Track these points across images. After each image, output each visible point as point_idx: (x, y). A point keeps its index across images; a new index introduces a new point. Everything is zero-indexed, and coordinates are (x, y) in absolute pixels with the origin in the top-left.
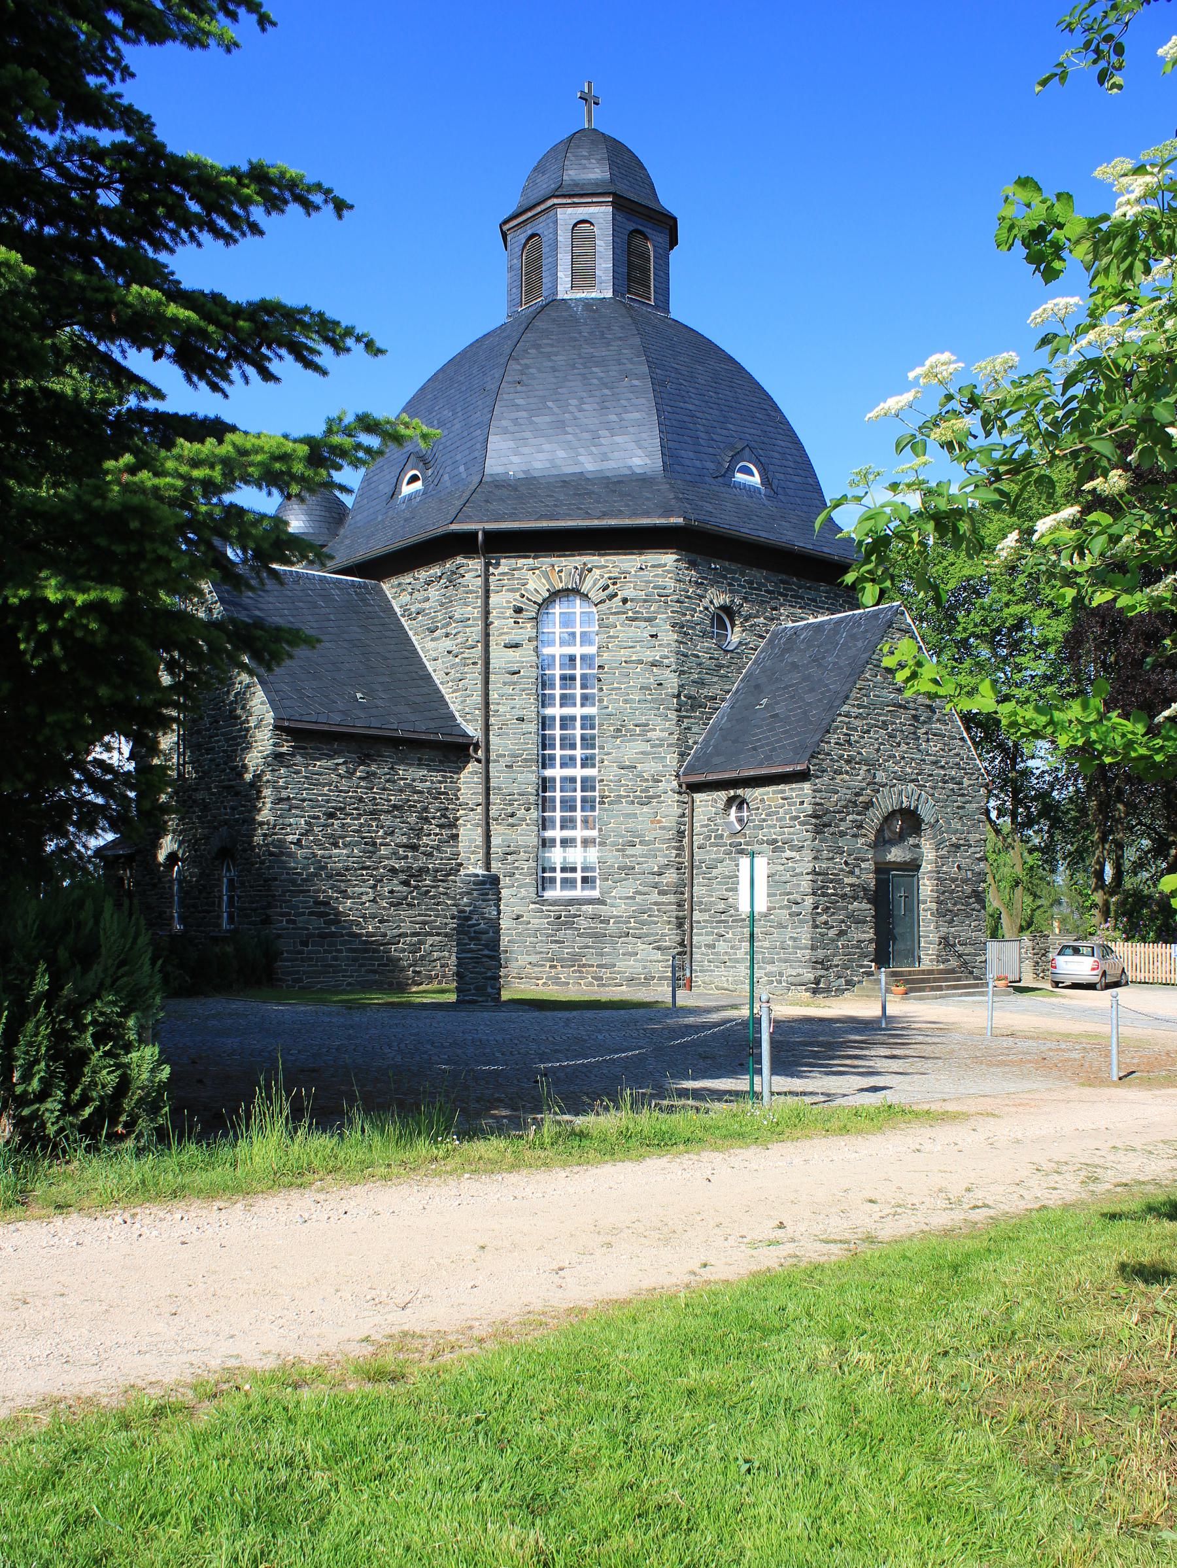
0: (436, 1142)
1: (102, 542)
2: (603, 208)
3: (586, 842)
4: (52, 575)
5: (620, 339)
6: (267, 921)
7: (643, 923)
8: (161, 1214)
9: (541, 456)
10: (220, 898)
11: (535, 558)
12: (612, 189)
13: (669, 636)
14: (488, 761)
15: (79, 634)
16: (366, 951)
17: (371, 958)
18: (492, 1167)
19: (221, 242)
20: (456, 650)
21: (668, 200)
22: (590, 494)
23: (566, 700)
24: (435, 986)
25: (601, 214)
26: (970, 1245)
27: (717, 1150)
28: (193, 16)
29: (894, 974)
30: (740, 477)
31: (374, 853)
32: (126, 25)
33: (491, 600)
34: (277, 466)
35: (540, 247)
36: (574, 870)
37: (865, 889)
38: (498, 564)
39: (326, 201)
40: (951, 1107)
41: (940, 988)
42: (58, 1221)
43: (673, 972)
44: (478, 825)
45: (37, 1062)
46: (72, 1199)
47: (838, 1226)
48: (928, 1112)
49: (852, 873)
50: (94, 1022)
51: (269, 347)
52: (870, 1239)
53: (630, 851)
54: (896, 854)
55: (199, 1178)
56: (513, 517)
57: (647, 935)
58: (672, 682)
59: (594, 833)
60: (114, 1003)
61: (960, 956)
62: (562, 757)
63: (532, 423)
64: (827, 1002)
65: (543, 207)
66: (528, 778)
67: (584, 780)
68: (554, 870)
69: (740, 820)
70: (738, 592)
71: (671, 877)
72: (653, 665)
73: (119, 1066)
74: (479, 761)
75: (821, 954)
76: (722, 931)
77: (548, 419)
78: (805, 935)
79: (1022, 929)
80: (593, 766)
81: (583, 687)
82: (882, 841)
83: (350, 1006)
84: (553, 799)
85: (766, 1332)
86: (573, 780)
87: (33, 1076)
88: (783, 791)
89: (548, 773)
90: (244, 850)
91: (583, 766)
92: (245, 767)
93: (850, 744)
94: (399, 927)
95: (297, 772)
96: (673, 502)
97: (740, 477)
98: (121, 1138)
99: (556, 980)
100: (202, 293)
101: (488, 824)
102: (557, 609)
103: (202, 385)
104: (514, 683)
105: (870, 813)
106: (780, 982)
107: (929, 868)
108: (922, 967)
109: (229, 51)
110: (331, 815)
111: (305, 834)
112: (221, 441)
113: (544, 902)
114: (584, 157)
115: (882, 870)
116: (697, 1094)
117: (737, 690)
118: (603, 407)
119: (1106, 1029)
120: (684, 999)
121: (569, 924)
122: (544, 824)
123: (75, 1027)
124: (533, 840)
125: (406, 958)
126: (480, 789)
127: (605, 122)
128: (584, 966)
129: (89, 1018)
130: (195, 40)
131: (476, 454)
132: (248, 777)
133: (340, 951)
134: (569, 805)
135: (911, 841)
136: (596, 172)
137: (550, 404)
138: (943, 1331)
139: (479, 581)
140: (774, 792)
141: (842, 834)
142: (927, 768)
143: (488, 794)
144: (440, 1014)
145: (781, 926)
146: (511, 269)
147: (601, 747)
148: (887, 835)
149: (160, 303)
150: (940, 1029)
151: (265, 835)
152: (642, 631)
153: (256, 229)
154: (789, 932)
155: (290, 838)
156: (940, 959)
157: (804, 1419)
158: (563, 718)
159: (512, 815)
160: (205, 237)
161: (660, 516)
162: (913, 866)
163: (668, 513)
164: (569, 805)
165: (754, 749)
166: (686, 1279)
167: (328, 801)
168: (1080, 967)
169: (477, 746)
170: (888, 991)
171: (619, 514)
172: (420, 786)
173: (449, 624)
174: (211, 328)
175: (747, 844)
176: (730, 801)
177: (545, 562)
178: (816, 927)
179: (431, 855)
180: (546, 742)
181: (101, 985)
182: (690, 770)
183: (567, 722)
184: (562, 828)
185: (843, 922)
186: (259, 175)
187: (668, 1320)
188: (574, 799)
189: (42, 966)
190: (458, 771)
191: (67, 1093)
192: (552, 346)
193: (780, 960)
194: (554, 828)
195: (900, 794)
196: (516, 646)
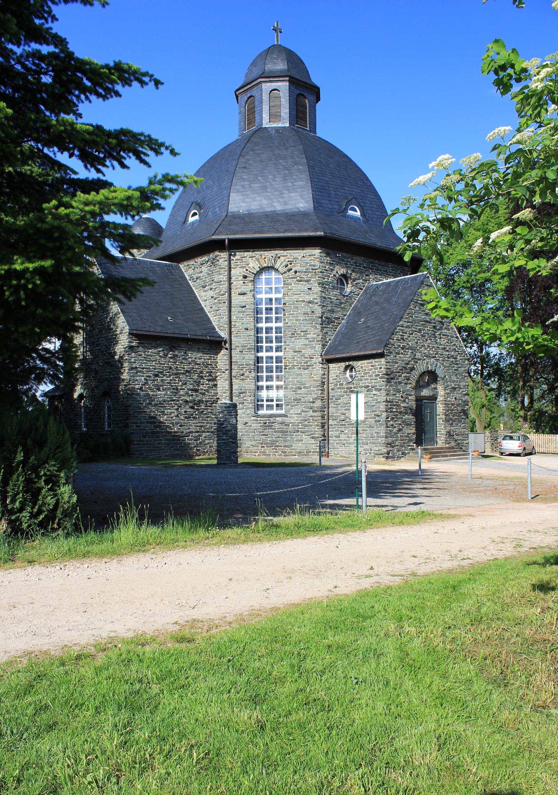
0: (208, 530)
1: (43, 241)
2: (284, 83)
3: (278, 387)
5: (293, 146)
6: (126, 426)
7: (305, 426)
8: (78, 565)
9: (255, 203)
10: (104, 415)
13: (317, 289)
14: (231, 349)
16: (174, 440)
18: (235, 542)
19: (101, 100)
20: (215, 296)
21: (315, 79)
23: (268, 320)
24: (206, 456)
25: (283, 86)
26: (461, 577)
27: (341, 533)
29: (425, 449)
30: (350, 212)
31: (177, 393)
33: (232, 272)
34: (125, 203)
35: (254, 102)
36: (272, 401)
37: (411, 409)
38: (235, 255)
40: (452, 512)
41: (446, 456)
42: (29, 569)
43: (320, 449)
44: (226, 380)
45: (18, 493)
46: (36, 558)
47: (398, 568)
48: (441, 515)
49: (404, 401)
50: (45, 475)
51: (124, 152)
52: (414, 574)
53: (299, 391)
54: (425, 392)
55: (96, 548)
56: (242, 232)
57: (307, 432)
58: (319, 311)
59: (282, 383)
60: (54, 466)
61: (456, 441)
62: (266, 347)
63: (251, 187)
64: (393, 463)
65: (255, 83)
66: (250, 357)
67: (277, 358)
68: (263, 401)
69: (351, 376)
70: (350, 267)
71: (318, 403)
72: (309, 303)
74: (227, 349)
75: (390, 440)
76: (343, 429)
77: (258, 185)
78: (382, 431)
79: (485, 428)
80: (281, 351)
81: (276, 313)
82: (419, 386)
83: (166, 466)
84: (262, 367)
85: (365, 618)
86: (271, 358)
88: (372, 363)
89: (260, 354)
90: (115, 393)
92: (115, 353)
93: (404, 340)
94: (189, 428)
95: (140, 355)
96: (319, 225)
97: (350, 212)
99: (264, 453)
101: (231, 379)
102: (264, 276)
103: (93, 170)
104: (243, 312)
105: (413, 372)
106: (370, 453)
107: (441, 399)
108: (438, 446)
109: (104, 6)
110: (156, 376)
113: (258, 416)
115: (419, 400)
116: (332, 507)
118: (285, 179)
119: (525, 475)
120: (325, 462)
121: (270, 427)
122: (258, 379)
123: (36, 477)
124: (253, 387)
125: (193, 443)
126: (227, 362)
128: (277, 446)
129: (43, 473)
131: (224, 202)
132: (117, 357)
133: (161, 440)
134: (269, 370)
135: (433, 386)
136: (281, 66)
137: (259, 178)
139: (226, 263)
140: (367, 363)
141: (400, 383)
143: (231, 365)
145: (371, 427)
146: (240, 113)
147: (285, 342)
150: (448, 475)
151: (125, 385)
152: (304, 286)
153: (118, 94)
154: (375, 430)
155: (137, 386)
156: (447, 442)
158: (267, 328)
159: (243, 375)
160: (93, 98)
161: (313, 231)
162: (434, 398)
163: (316, 230)
164: (269, 370)
165: (358, 342)
166: (327, 593)
167: (155, 369)
169: (226, 342)
170: (422, 457)
171: (292, 230)
172: (199, 361)
173: (212, 284)
175: (355, 388)
176: (346, 368)
177: (257, 254)
178: (388, 427)
179: (204, 394)
180: (258, 340)
181: (48, 457)
183: (268, 330)
184: (267, 381)
185: (400, 424)
187: (319, 613)
188: (272, 367)
189: (20, 448)
190: (217, 353)
191: (32, 508)
192: (260, 150)
193: (370, 443)
194: (263, 381)
195: (427, 363)
196: (244, 294)
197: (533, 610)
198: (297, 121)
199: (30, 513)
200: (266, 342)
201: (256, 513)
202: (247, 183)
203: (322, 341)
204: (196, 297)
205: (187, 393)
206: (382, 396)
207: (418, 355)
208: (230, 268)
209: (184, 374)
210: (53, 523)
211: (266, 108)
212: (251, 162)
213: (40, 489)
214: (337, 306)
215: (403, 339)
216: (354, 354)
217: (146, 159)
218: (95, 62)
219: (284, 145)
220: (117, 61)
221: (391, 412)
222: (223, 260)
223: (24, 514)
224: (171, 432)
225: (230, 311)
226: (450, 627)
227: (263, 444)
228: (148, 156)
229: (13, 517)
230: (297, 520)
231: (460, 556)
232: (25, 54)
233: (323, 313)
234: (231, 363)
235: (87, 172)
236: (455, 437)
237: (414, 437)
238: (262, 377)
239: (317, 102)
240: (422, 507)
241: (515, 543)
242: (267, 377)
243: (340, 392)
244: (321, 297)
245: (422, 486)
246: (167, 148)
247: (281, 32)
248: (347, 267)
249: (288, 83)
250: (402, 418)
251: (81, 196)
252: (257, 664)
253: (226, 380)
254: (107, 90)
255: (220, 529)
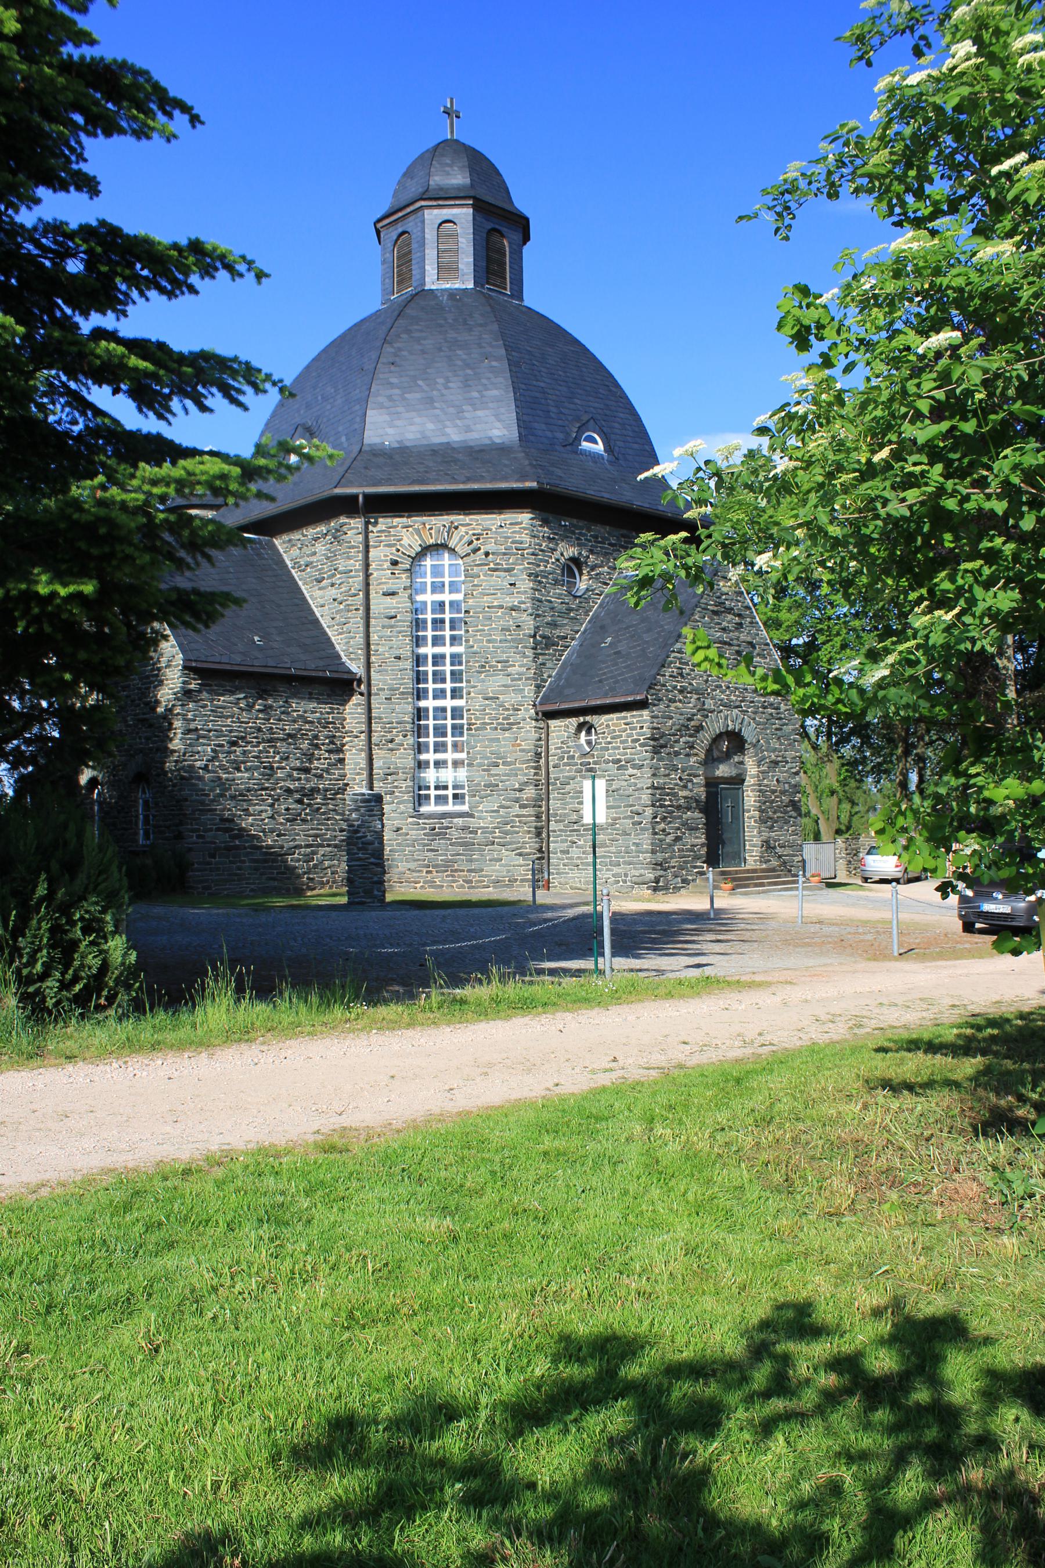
0: (349, 1007)
1: (82, 545)
2: (464, 210)
3: (456, 764)
4: (44, 572)
5: (481, 325)
6: (179, 836)
7: (506, 833)
8: (146, 1062)
9: (413, 428)
10: (137, 816)
11: (409, 517)
12: (472, 193)
13: (525, 585)
14: (370, 695)
15: (65, 616)
16: (266, 861)
17: (271, 868)
18: (393, 1025)
19: (164, 298)
20: (340, 598)
21: (521, 202)
22: (455, 461)
23: (437, 641)
24: (326, 890)
25: (463, 215)
26: (750, 1067)
27: (568, 1010)
28: (142, 116)
29: (723, 873)
30: (585, 445)
31: (271, 775)
32: (86, 122)
33: (371, 554)
34: (218, 483)
35: (409, 244)
36: (446, 788)
37: (697, 801)
38: (376, 523)
39: (249, 270)
40: (758, 978)
41: (762, 885)
42: (70, 1068)
43: (533, 875)
44: (362, 750)
45: (40, 950)
46: (76, 1052)
47: (658, 1059)
48: (738, 982)
49: (685, 787)
50: (82, 919)
51: (204, 387)
52: (681, 1066)
53: (494, 771)
54: (723, 770)
55: (170, 1036)
56: (389, 482)
57: (510, 843)
58: (529, 624)
59: (463, 756)
60: (97, 903)
61: (780, 857)
62: (434, 690)
63: (405, 399)
64: (666, 898)
65: (412, 208)
66: (405, 709)
67: (454, 710)
68: (428, 788)
69: (589, 743)
70: (585, 545)
71: (530, 792)
72: (512, 609)
73: (101, 952)
74: (362, 694)
75: (660, 856)
76: (574, 838)
77: (418, 396)
78: (646, 840)
79: (838, 832)
80: (461, 697)
81: (452, 628)
82: (711, 759)
83: (257, 909)
84: (427, 727)
85: (598, 1119)
86: (444, 710)
87: (36, 961)
88: (625, 718)
89: (422, 704)
90: (158, 775)
91: (453, 697)
92: (158, 702)
93: (683, 677)
94: (294, 840)
95: (204, 706)
96: (528, 468)
97: (585, 445)
98: (103, 1008)
99: (432, 884)
100: (149, 341)
101: (370, 749)
102: (428, 562)
103: (151, 414)
104: (392, 627)
105: (700, 735)
106: (625, 882)
107: (752, 781)
108: (748, 867)
109: (168, 141)
110: (234, 744)
111: (212, 760)
112: (174, 463)
113: (420, 816)
114: (448, 165)
115: (712, 784)
116: (552, 972)
117: (585, 630)
118: (466, 385)
119: (887, 915)
120: (543, 897)
121: (442, 835)
122: (420, 748)
123: (67, 923)
124: (410, 762)
125: (301, 867)
126: (363, 718)
127: (465, 133)
128: (456, 871)
129: (78, 916)
130: (142, 133)
131: (356, 426)
132: (160, 710)
133: (244, 862)
134: (440, 731)
135: (736, 759)
136: (458, 178)
137: (420, 382)
138: (722, 1117)
139: (360, 538)
140: (618, 719)
141: (677, 754)
142: (749, 696)
143: (370, 723)
144: (334, 914)
145: (625, 833)
146: (384, 262)
147: (468, 681)
148: (716, 754)
149: (123, 356)
150: (763, 918)
151: (176, 761)
152: (501, 580)
153: (192, 290)
154: (633, 839)
155: (198, 764)
156: (763, 860)
157: (620, 1167)
158: (434, 657)
159: (392, 741)
160: (153, 294)
161: (517, 481)
162: (738, 780)
163: (523, 478)
164: (440, 731)
165: (600, 681)
166: (543, 1093)
167: (231, 731)
168: (884, 863)
169: (360, 682)
170: (715, 887)
171: (480, 479)
172: (310, 717)
173: (334, 575)
174: (162, 372)
175: (595, 763)
176: (580, 727)
177: (417, 521)
178: (656, 834)
179: (321, 777)
180: (420, 677)
181: (86, 888)
182: (545, 700)
183: (438, 659)
184: (435, 751)
186: (196, 247)
187: (531, 1114)
188: (445, 726)
189: (43, 876)
190: (344, 702)
191: (63, 974)
192: (421, 331)
193: (625, 863)
194: (428, 751)
195: (726, 718)
196: (393, 594)
197: (852, 1106)
198: (488, 278)
199: (58, 981)
200: (435, 682)
201: (425, 982)
202: (397, 391)
203: (536, 680)
204: (304, 598)
205: (290, 776)
206: (645, 779)
207: (709, 704)
208: (367, 548)
209: (283, 740)
210: (99, 997)
211: (431, 254)
212: (405, 353)
213: (75, 944)
214: (563, 614)
215: (681, 675)
216: (593, 703)
217: (241, 398)
218: (157, 239)
219: (465, 323)
220: (193, 237)
221: (661, 806)
222: (355, 531)
223: (49, 984)
224: (262, 847)
225: (367, 625)
226: (723, 1129)
227: (430, 867)
228: (244, 393)
229: (31, 989)
230: (495, 991)
231: (761, 1040)
232: (41, 227)
233: (537, 628)
234: (370, 719)
235: (141, 417)
236: (778, 850)
237: (704, 851)
238: (427, 745)
239: (525, 243)
240: (708, 971)
241: (851, 1023)
242: (436, 744)
243: (570, 771)
244: (533, 599)
245: (713, 937)
246: (274, 384)
247: (458, 117)
248: (579, 545)
249: (471, 210)
250: (681, 817)
251: (146, 469)
252: (443, 1174)
253: (362, 750)
254: (174, 282)
255: (368, 1005)
